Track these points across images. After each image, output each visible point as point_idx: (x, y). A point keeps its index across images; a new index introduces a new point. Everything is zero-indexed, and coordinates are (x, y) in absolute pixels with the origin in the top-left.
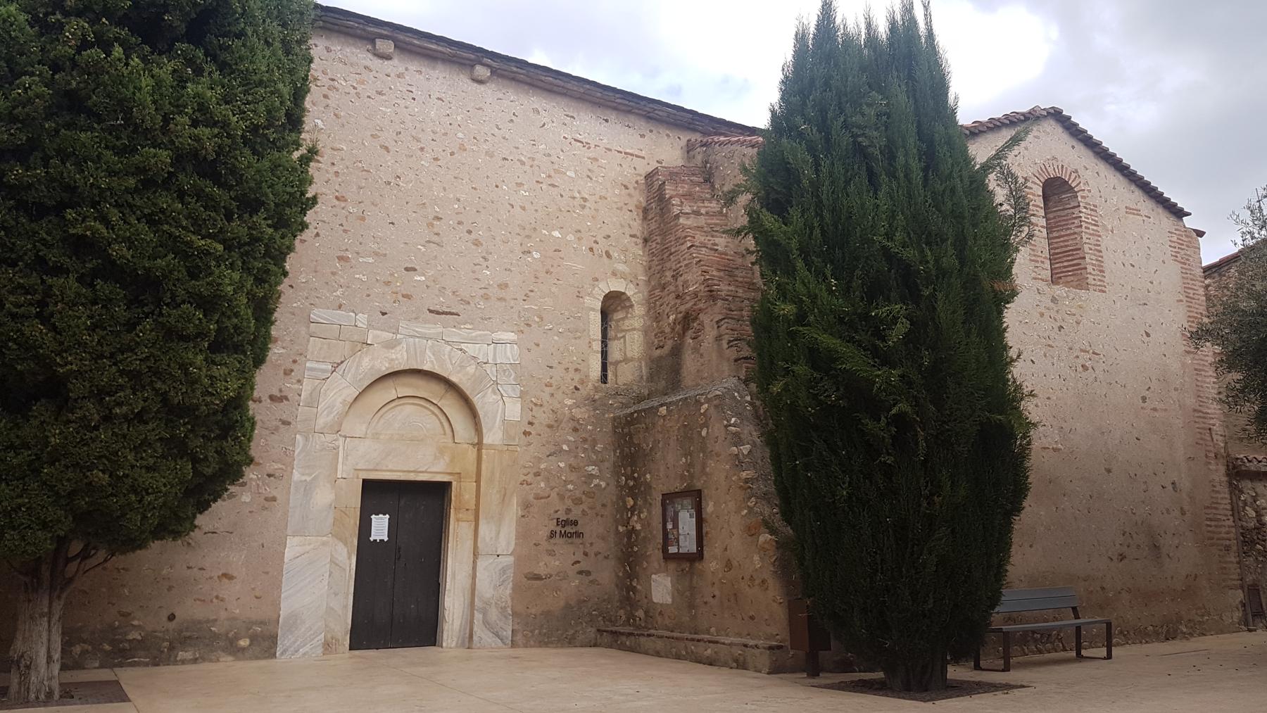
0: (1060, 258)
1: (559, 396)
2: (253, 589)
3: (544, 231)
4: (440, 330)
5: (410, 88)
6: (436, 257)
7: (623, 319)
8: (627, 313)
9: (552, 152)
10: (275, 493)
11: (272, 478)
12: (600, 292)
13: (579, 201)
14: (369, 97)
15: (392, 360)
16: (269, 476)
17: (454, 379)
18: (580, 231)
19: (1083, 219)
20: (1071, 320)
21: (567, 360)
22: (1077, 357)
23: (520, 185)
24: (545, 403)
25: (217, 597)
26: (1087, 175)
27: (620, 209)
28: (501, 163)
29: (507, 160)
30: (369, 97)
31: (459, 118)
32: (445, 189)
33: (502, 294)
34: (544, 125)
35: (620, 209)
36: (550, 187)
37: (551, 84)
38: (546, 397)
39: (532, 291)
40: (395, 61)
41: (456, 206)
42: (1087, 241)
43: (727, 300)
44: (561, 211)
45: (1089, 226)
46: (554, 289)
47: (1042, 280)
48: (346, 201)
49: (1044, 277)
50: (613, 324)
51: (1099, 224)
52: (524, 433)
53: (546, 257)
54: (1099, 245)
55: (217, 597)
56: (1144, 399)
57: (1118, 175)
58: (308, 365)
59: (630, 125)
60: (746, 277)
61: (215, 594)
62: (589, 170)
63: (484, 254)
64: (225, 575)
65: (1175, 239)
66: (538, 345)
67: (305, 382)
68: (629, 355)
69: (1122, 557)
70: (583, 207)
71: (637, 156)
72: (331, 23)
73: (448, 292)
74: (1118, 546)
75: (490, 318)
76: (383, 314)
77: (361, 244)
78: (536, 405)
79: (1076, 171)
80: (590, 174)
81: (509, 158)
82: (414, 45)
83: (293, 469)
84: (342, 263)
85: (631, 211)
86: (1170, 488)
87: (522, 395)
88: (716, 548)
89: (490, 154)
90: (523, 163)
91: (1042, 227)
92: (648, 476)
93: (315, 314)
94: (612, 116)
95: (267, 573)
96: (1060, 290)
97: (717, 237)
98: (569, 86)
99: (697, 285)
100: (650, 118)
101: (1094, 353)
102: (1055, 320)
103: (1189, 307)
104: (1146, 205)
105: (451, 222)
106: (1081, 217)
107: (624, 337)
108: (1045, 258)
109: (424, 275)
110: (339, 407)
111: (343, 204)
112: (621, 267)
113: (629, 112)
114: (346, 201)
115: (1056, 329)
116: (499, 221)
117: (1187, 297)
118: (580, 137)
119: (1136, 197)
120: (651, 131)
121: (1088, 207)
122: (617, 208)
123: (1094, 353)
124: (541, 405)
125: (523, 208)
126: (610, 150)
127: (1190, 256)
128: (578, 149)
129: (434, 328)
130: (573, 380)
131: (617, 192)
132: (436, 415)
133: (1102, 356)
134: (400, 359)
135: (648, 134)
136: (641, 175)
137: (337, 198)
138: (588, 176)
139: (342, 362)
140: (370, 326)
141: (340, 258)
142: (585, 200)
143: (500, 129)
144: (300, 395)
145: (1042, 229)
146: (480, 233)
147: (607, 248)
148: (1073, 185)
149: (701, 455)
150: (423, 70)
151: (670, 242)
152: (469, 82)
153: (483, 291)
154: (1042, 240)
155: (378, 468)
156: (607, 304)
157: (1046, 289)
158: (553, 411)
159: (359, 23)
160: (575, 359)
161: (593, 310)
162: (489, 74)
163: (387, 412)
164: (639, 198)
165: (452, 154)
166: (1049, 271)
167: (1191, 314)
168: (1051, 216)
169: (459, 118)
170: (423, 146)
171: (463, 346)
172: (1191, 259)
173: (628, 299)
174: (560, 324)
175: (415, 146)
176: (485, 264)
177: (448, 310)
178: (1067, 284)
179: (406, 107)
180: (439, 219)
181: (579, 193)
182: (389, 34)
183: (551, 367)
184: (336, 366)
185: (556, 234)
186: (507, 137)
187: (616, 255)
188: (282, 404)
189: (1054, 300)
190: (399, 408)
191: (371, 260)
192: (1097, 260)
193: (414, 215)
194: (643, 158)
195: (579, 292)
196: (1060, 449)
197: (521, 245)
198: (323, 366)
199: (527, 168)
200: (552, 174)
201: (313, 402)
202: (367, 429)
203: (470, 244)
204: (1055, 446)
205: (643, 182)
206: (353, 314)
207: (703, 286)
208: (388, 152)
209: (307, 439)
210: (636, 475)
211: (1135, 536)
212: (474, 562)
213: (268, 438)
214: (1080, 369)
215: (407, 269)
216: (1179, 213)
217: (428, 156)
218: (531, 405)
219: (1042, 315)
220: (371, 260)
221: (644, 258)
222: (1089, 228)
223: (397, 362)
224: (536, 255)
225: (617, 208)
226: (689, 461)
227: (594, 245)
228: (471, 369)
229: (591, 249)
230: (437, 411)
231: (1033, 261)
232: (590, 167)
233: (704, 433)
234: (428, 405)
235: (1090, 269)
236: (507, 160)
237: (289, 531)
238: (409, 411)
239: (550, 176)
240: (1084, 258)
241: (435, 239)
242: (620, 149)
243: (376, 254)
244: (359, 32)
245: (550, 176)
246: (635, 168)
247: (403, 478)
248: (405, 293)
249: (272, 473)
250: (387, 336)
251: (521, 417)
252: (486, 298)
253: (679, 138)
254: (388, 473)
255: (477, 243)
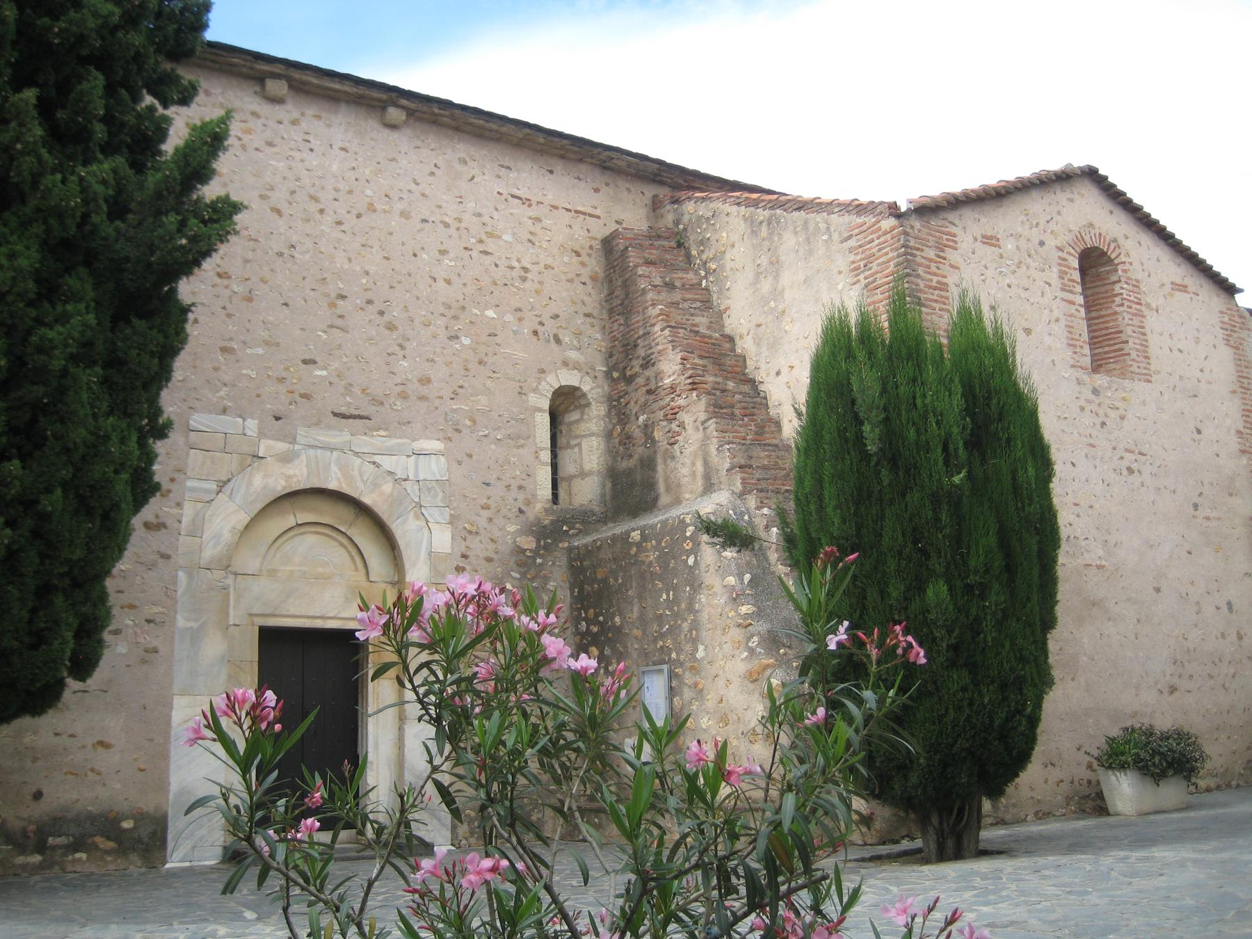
0: (1100, 342)
1: (499, 521)
2: (136, 760)
3: (475, 311)
4: (348, 438)
5: (307, 137)
6: (340, 345)
7: (577, 421)
8: (583, 413)
9: (484, 211)
10: (155, 643)
11: (152, 624)
12: (548, 387)
13: (517, 273)
14: (257, 149)
15: (290, 477)
16: (149, 621)
17: (367, 500)
18: (520, 310)
19: (1125, 296)
20: (1113, 414)
21: (508, 475)
22: (1122, 458)
23: (443, 252)
24: (482, 531)
25: (92, 770)
26: (1127, 245)
27: (570, 281)
28: (420, 226)
29: (427, 221)
30: (257, 149)
31: (367, 172)
32: (350, 260)
33: (424, 390)
34: (473, 178)
35: (570, 281)
36: (482, 256)
37: (482, 127)
38: (482, 522)
39: (461, 387)
40: (289, 106)
41: (364, 281)
42: (1130, 322)
43: (714, 395)
44: (496, 284)
45: (1131, 304)
46: (489, 383)
47: (1082, 368)
48: (229, 277)
49: (1084, 365)
50: (564, 428)
51: (1143, 302)
52: (456, 569)
53: (477, 343)
54: (1143, 327)
55: (92, 770)
56: (1196, 506)
57: (1162, 243)
58: (190, 483)
59: (581, 176)
60: (737, 366)
61: (90, 766)
62: (531, 233)
63: (400, 341)
64: (101, 743)
65: (1226, 319)
66: (470, 456)
67: (187, 505)
68: (587, 467)
69: (1173, 690)
70: (524, 279)
71: (591, 215)
72: (212, 61)
73: (356, 390)
74: (1168, 677)
75: (409, 423)
76: (278, 419)
77: (248, 331)
78: (470, 532)
79: (1115, 240)
80: (531, 237)
81: (430, 220)
82: (313, 84)
83: (176, 612)
84: (227, 356)
85: (584, 284)
86: (1225, 608)
87: (453, 520)
88: (708, 700)
89: (405, 215)
90: (447, 225)
91: (1080, 305)
92: (617, 619)
93: (195, 421)
94: (559, 166)
95: (152, 740)
96: (1101, 380)
97: (698, 316)
98: (504, 130)
99: (675, 376)
100: (606, 168)
101: (1141, 454)
102: (1097, 414)
103: (1244, 399)
104: (1194, 281)
105: (358, 301)
106: (1122, 294)
107: (579, 445)
108: (1084, 342)
109: (325, 368)
110: (227, 536)
111: (226, 282)
112: (574, 355)
113: (581, 161)
114: (229, 277)
115: (1099, 426)
116: (418, 298)
117: (1242, 387)
118: (518, 193)
119: (1174, 270)
120: (607, 184)
121: (1130, 282)
122: (568, 281)
123: (1141, 454)
124: (477, 533)
125: (448, 282)
126: (556, 208)
127: (1243, 339)
128: (517, 208)
129: (339, 435)
130: (516, 500)
131: (566, 259)
132: (345, 547)
133: (1149, 457)
134: (300, 475)
135: (604, 189)
136: (596, 239)
137: (219, 275)
138: (530, 241)
139: (229, 480)
140: (262, 434)
141: (224, 350)
142: (526, 270)
143: (418, 184)
144: (180, 522)
145: (1080, 308)
146: (395, 314)
147: (555, 331)
148: (1113, 256)
149: (688, 589)
150: (323, 114)
151: (638, 322)
152: (379, 127)
153: (400, 388)
154: (1080, 321)
155: (276, 613)
156: (557, 402)
157: (1086, 378)
158: (492, 540)
159: (246, 61)
160: (518, 473)
161: (540, 410)
162: (404, 118)
163: (284, 543)
164: (595, 265)
165: (359, 216)
166: (1089, 358)
167: (1246, 407)
168: (1089, 292)
169: (367, 172)
170: (322, 207)
171: (377, 459)
172: (1245, 343)
173: (584, 395)
174: (498, 428)
175: (313, 207)
176: (401, 353)
177: (356, 413)
178: (1109, 372)
179: (302, 161)
180: (343, 297)
181: (519, 261)
182: (282, 72)
183: (488, 484)
184: (222, 485)
185: (490, 313)
186: (427, 193)
187: (567, 339)
188: (159, 533)
189: (1095, 392)
190: (299, 538)
191: (260, 351)
192: (1141, 345)
193: (312, 293)
194: (598, 217)
195: (521, 387)
196: (1104, 566)
197: (447, 328)
198: (206, 485)
199: (452, 231)
200: (484, 237)
201: (196, 530)
202: (262, 564)
203: (382, 329)
204: (1098, 563)
205: (599, 247)
206: (240, 420)
207: (683, 378)
208: (281, 216)
209: (190, 576)
210: (601, 618)
211: (1186, 664)
212: (401, 729)
213: (145, 576)
214: (1125, 472)
215: (305, 362)
216: (1229, 289)
217: (329, 218)
218: (464, 533)
219: (1082, 409)
220: (260, 351)
221: (603, 344)
222: (1131, 307)
223: (295, 479)
224: (466, 341)
225: (568, 281)
226: (671, 597)
227: (540, 328)
228: (388, 487)
229: (535, 333)
230: (345, 541)
231: (1071, 345)
232: (532, 229)
233: (691, 561)
234: (334, 534)
235: (1134, 355)
236: (427, 221)
237: (176, 688)
238: (310, 542)
239: (481, 241)
240: (1127, 342)
241: (339, 322)
242: (569, 207)
243: (267, 343)
244: (245, 70)
245: (481, 241)
246: (588, 230)
247: (307, 626)
248: (303, 391)
249: (152, 618)
250: (281, 446)
251: (452, 548)
252: (404, 396)
253: (642, 193)
254: (290, 620)
255: (391, 327)
